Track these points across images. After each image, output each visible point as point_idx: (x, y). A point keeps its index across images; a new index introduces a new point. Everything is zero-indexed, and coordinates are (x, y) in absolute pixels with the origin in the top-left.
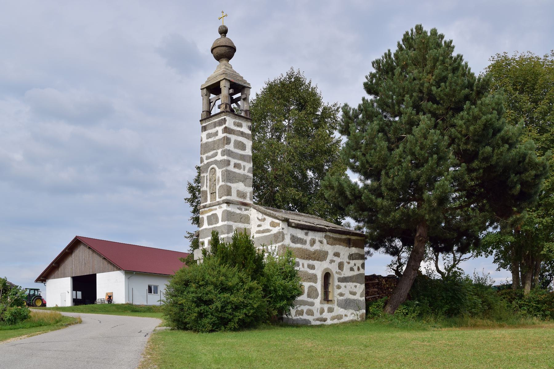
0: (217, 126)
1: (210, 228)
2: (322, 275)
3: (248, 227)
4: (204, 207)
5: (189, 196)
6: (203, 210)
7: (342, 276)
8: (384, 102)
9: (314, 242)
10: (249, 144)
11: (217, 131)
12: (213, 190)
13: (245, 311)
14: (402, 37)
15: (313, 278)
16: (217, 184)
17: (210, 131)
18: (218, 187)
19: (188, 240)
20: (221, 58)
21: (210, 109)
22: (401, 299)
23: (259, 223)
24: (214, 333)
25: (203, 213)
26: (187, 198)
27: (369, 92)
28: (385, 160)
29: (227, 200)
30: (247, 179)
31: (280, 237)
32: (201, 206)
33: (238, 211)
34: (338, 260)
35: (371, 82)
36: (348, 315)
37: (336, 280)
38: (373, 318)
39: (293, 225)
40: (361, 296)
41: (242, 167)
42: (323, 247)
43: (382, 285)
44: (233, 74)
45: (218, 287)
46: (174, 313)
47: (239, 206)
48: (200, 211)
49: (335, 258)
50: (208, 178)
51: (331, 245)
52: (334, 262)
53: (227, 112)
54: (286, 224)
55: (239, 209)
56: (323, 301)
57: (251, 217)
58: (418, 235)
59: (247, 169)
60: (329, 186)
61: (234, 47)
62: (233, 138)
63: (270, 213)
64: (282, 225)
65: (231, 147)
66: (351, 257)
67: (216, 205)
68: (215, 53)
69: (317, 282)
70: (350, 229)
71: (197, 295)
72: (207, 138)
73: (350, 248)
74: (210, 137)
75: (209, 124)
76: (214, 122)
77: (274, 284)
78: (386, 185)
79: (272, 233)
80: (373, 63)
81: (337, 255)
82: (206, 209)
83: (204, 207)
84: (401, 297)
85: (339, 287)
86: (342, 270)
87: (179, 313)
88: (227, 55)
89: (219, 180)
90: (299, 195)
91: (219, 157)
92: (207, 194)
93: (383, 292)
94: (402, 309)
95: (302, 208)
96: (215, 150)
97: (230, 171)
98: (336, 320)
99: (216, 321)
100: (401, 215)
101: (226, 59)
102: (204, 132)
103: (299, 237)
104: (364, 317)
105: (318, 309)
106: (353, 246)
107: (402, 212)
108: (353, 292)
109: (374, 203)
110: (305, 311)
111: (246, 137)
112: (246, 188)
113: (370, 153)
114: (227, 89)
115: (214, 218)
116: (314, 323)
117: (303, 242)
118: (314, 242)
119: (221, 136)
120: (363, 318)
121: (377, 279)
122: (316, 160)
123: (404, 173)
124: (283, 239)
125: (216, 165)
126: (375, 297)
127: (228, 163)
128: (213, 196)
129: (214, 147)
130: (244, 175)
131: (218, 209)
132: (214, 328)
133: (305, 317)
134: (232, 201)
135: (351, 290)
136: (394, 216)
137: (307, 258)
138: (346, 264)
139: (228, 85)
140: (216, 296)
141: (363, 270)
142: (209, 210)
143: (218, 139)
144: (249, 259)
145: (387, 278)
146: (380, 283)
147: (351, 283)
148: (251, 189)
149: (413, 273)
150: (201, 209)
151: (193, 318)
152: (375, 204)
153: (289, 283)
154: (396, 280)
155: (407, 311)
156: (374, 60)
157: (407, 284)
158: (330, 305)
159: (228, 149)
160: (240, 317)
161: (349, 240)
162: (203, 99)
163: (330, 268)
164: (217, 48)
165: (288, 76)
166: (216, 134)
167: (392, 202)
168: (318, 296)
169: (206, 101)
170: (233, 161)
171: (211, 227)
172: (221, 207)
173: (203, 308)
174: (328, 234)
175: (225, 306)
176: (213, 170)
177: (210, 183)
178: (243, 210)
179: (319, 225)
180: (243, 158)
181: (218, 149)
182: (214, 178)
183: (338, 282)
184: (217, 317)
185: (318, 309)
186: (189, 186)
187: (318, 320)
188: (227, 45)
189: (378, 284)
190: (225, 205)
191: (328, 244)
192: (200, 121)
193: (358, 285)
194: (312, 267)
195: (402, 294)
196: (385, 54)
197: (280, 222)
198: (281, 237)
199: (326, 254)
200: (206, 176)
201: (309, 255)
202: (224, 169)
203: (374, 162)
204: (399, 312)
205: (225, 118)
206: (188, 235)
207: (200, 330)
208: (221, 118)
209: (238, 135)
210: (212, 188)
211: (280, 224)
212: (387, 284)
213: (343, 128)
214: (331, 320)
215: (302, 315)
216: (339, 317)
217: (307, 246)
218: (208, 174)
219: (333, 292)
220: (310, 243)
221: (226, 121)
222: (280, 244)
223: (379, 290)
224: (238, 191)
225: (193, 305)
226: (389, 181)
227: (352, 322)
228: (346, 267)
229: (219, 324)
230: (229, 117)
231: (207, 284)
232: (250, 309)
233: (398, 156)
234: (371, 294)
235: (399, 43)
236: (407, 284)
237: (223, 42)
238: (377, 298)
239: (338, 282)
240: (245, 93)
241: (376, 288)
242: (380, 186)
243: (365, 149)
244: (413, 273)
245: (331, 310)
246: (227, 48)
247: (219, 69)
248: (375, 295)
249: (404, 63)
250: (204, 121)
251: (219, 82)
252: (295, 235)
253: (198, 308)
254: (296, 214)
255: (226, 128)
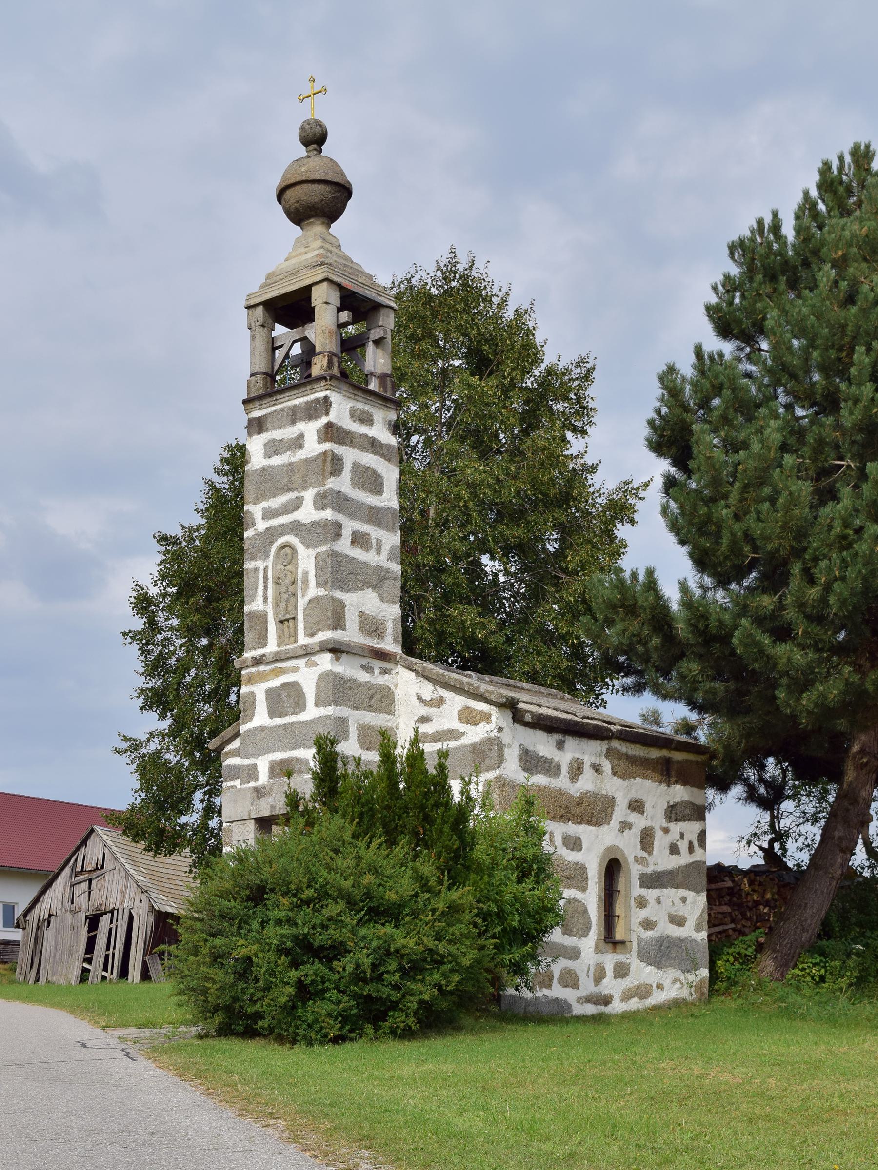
0: (301, 419)
1: (276, 727)
2: (600, 866)
3: (390, 724)
4: (258, 661)
5: (138, 624)
6: (253, 670)
7: (649, 870)
8: (783, 365)
9: (579, 768)
10: (390, 474)
11: (301, 436)
12: (287, 611)
13: (436, 976)
14: (817, 177)
15: (578, 875)
16: (299, 595)
17: (276, 434)
18: (302, 603)
19: (125, 759)
20: (309, 217)
21: (273, 367)
22: (805, 936)
23: (424, 711)
24: (348, 1045)
25: (251, 680)
26: (130, 632)
27: (724, 329)
28: (801, 534)
29: (335, 641)
30: (386, 578)
31: (491, 754)
32: (246, 659)
33: (363, 677)
34: (639, 822)
35: (731, 303)
36: (665, 985)
37: (636, 882)
38: (727, 992)
39: (528, 718)
40: (698, 929)
41: (374, 542)
42: (602, 782)
43: (741, 895)
44: (345, 265)
45: (357, 907)
46: (218, 986)
47: (364, 661)
48: (243, 672)
49: (633, 817)
50: (270, 574)
51: (623, 777)
52: (630, 829)
53: (332, 377)
54: (509, 714)
55: (368, 669)
56: (602, 945)
57: (399, 693)
58: (856, 748)
59: (386, 549)
60: (623, 606)
61: (347, 185)
62: (350, 455)
63: (461, 683)
64: (498, 718)
65: (343, 483)
66: (671, 812)
67: (297, 657)
68: (292, 201)
69: (587, 888)
70: (661, 730)
71: (294, 930)
72: (268, 456)
73: (668, 786)
74: (277, 453)
75: (275, 411)
76: (289, 408)
77: (497, 893)
78: (801, 606)
79: (465, 741)
80: (732, 248)
81: (637, 806)
82: (262, 668)
83: (258, 661)
84: (803, 930)
85: (642, 903)
86: (650, 853)
87: (233, 985)
88: (327, 210)
89: (306, 582)
90: (484, 627)
91: (308, 513)
92: (266, 622)
93: (743, 914)
94: (811, 967)
95: (439, 659)
96: (292, 490)
97: (341, 555)
98: (635, 999)
99: (350, 1008)
100: (843, 693)
101: (322, 220)
102: (256, 437)
103: (541, 754)
104: (706, 991)
105: (589, 969)
106: (676, 782)
107: (847, 683)
108: (676, 916)
109: (767, 656)
110: (556, 975)
111: (383, 456)
112: (384, 605)
113: (758, 513)
114: (331, 310)
115: (289, 696)
116: (579, 1010)
117: (550, 768)
118: (579, 768)
119: (313, 451)
120: (703, 994)
121: (727, 879)
122: (528, 522)
123: (860, 572)
124: (501, 760)
125: (296, 535)
126: (725, 931)
127: (336, 531)
128: (286, 630)
129: (291, 482)
130: (379, 568)
131: (304, 670)
132: (344, 1031)
133: (557, 992)
134: (349, 646)
135: (673, 911)
136: (823, 696)
137: (562, 816)
138: (659, 834)
139: (335, 298)
140: (353, 932)
141: (702, 851)
142: (272, 671)
143: (304, 457)
144: (439, 821)
145: (752, 875)
146: (735, 890)
147: (673, 890)
148: (394, 611)
149: (840, 860)
150: (247, 666)
151: (283, 1000)
152: (770, 661)
153: (536, 892)
154: (777, 881)
155: (823, 971)
156: (735, 238)
157: (822, 893)
158: (619, 957)
159: (337, 489)
160: (426, 997)
161: (668, 761)
162: (253, 338)
163: (621, 846)
164: (298, 188)
165: (439, 274)
166: (298, 442)
167: (817, 656)
168: (589, 928)
169: (261, 345)
170: (350, 526)
171: (278, 721)
172: (315, 664)
173: (311, 970)
174: (616, 744)
175: (380, 964)
176: (287, 550)
177: (275, 591)
178: (377, 671)
179: (588, 718)
180: (374, 516)
181: (305, 488)
182: (289, 575)
183: (641, 886)
184: (355, 996)
185: (589, 969)
186: (135, 594)
187: (589, 999)
188: (329, 178)
189: (731, 892)
190: (329, 656)
191: (614, 773)
192: (245, 402)
193: (690, 894)
194: (574, 844)
195: (806, 920)
196: (760, 222)
197: (493, 709)
198: (494, 754)
199: (610, 802)
200: (262, 568)
201: (567, 807)
202: (325, 548)
203: (768, 539)
204: (800, 973)
205: (326, 398)
206: (125, 745)
207: (299, 1038)
208: (312, 397)
209: (362, 448)
210: (283, 605)
211: (490, 715)
212: (754, 891)
213: (662, 436)
214: (622, 1000)
215: (549, 986)
216: (643, 992)
217: (562, 782)
218: (270, 563)
219: (628, 916)
220: (570, 771)
221: (330, 405)
222: (491, 775)
223: (734, 910)
224: (362, 614)
225: (280, 962)
226: (814, 593)
227: (676, 1004)
228: (661, 842)
229: (359, 1016)
230: (338, 395)
231: (323, 895)
232: (452, 971)
233: (837, 523)
234: (717, 923)
235: (806, 194)
236: (822, 893)
237: (315, 168)
238: (731, 932)
239: (641, 886)
240: (381, 323)
241: (726, 904)
242: (781, 606)
243: (741, 500)
244: (840, 860)
245: (621, 971)
246: (328, 188)
247: (303, 250)
248: (726, 924)
249: (840, 253)
250: (257, 403)
251: (307, 289)
252: (531, 748)
253: (296, 969)
254: (507, 685)
255: (329, 426)
